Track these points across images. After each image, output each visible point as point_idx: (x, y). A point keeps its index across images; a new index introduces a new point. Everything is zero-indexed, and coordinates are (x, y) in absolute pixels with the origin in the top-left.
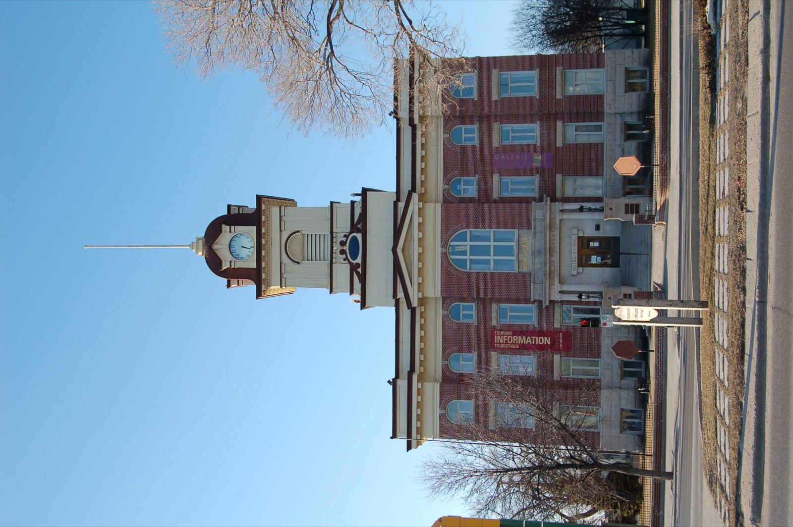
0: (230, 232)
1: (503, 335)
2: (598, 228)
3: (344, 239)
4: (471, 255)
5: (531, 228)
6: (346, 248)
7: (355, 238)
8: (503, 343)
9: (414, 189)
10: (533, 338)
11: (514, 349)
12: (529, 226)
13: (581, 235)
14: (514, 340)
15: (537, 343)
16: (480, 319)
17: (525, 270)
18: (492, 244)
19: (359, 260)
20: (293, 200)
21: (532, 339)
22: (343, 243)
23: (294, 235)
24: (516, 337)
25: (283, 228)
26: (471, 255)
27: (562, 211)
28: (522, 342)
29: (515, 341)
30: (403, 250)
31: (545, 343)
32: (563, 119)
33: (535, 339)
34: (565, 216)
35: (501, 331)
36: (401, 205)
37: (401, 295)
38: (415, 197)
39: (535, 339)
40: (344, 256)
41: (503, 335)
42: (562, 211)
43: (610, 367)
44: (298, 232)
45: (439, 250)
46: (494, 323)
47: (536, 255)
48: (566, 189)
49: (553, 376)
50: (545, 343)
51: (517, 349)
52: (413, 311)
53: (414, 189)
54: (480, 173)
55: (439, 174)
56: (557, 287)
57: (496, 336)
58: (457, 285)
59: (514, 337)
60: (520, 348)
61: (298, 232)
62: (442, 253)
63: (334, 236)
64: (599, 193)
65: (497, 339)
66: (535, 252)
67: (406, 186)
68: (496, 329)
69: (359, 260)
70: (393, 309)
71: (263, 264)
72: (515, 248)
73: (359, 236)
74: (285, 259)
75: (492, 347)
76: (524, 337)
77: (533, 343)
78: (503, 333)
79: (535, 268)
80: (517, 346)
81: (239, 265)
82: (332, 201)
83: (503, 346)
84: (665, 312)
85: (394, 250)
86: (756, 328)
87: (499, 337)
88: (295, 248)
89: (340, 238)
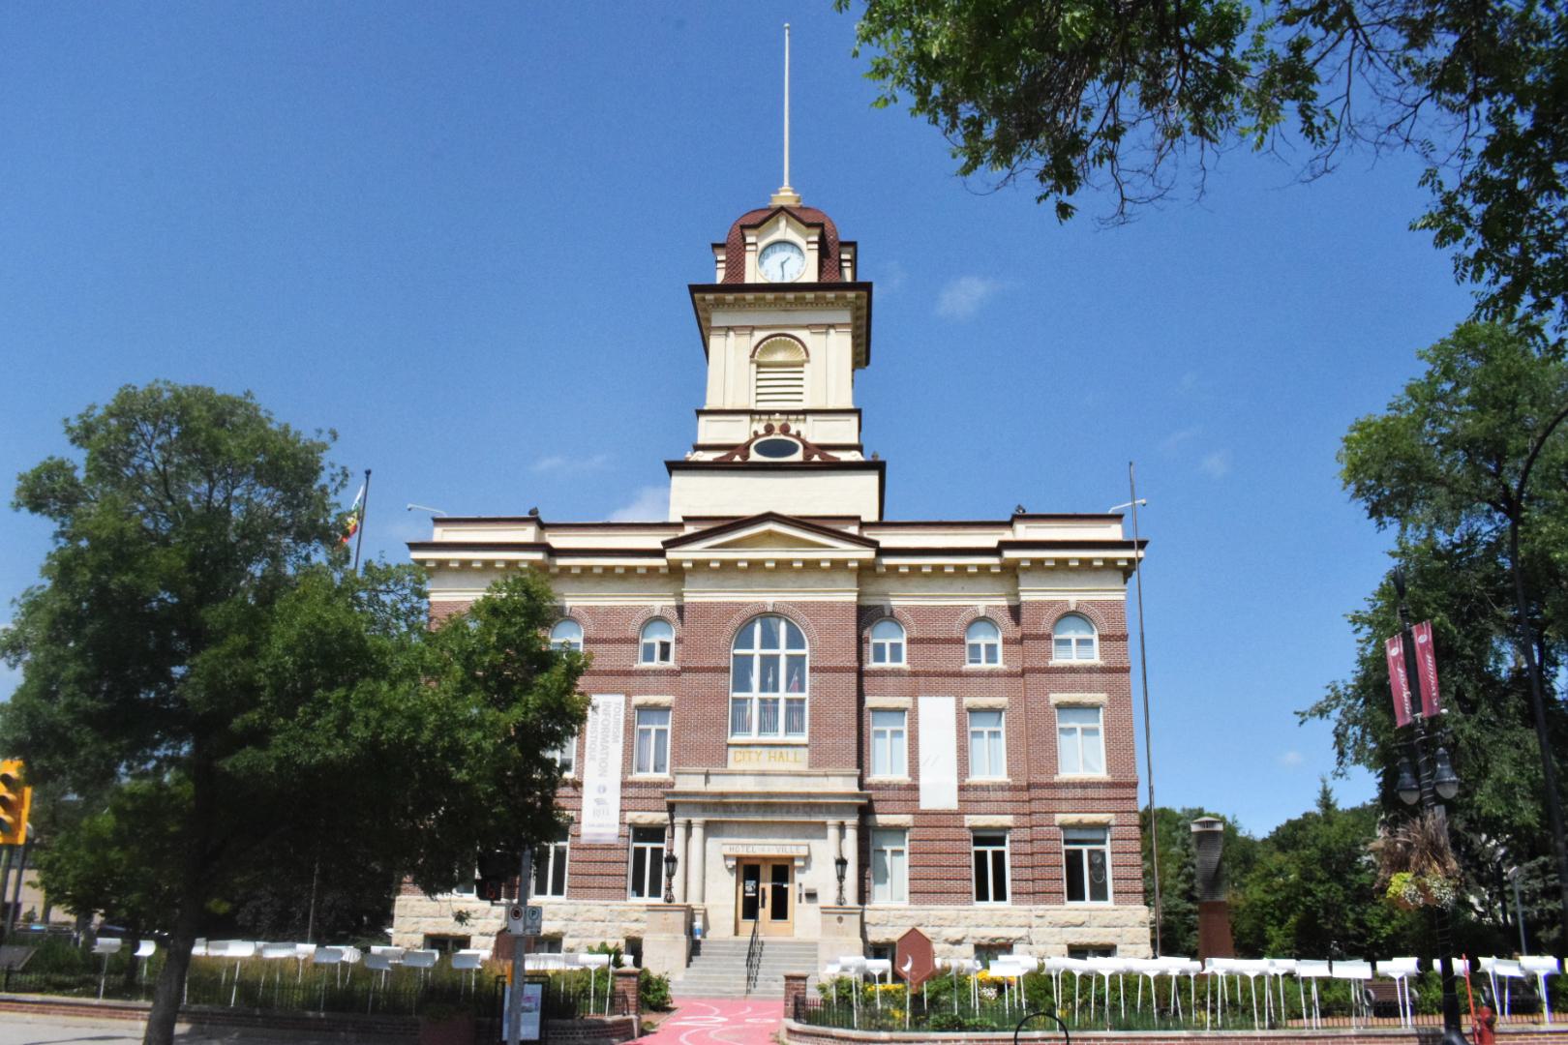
2: (812, 896)
3: (793, 431)
4: (763, 657)
6: (777, 436)
7: (793, 449)
12: (814, 763)
13: (797, 863)
17: (736, 760)
18: (782, 695)
19: (754, 457)
20: (867, 363)
22: (785, 430)
26: (763, 657)
27: (842, 827)
30: (770, 534)
34: (833, 833)
36: (853, 530)
37: (689, 530)
38: (869, 554)
40: (762, 431)
42: (842, 827)
48: (720, 778)
52: (995, 552)
53: (882, 552)
54: (915, 674)
64: (679, 481)
71: (750, 296)
73: (798, 457)
74: (759, 335)
81: (750, 259)
82: (875, 289)
86: (814, 819)
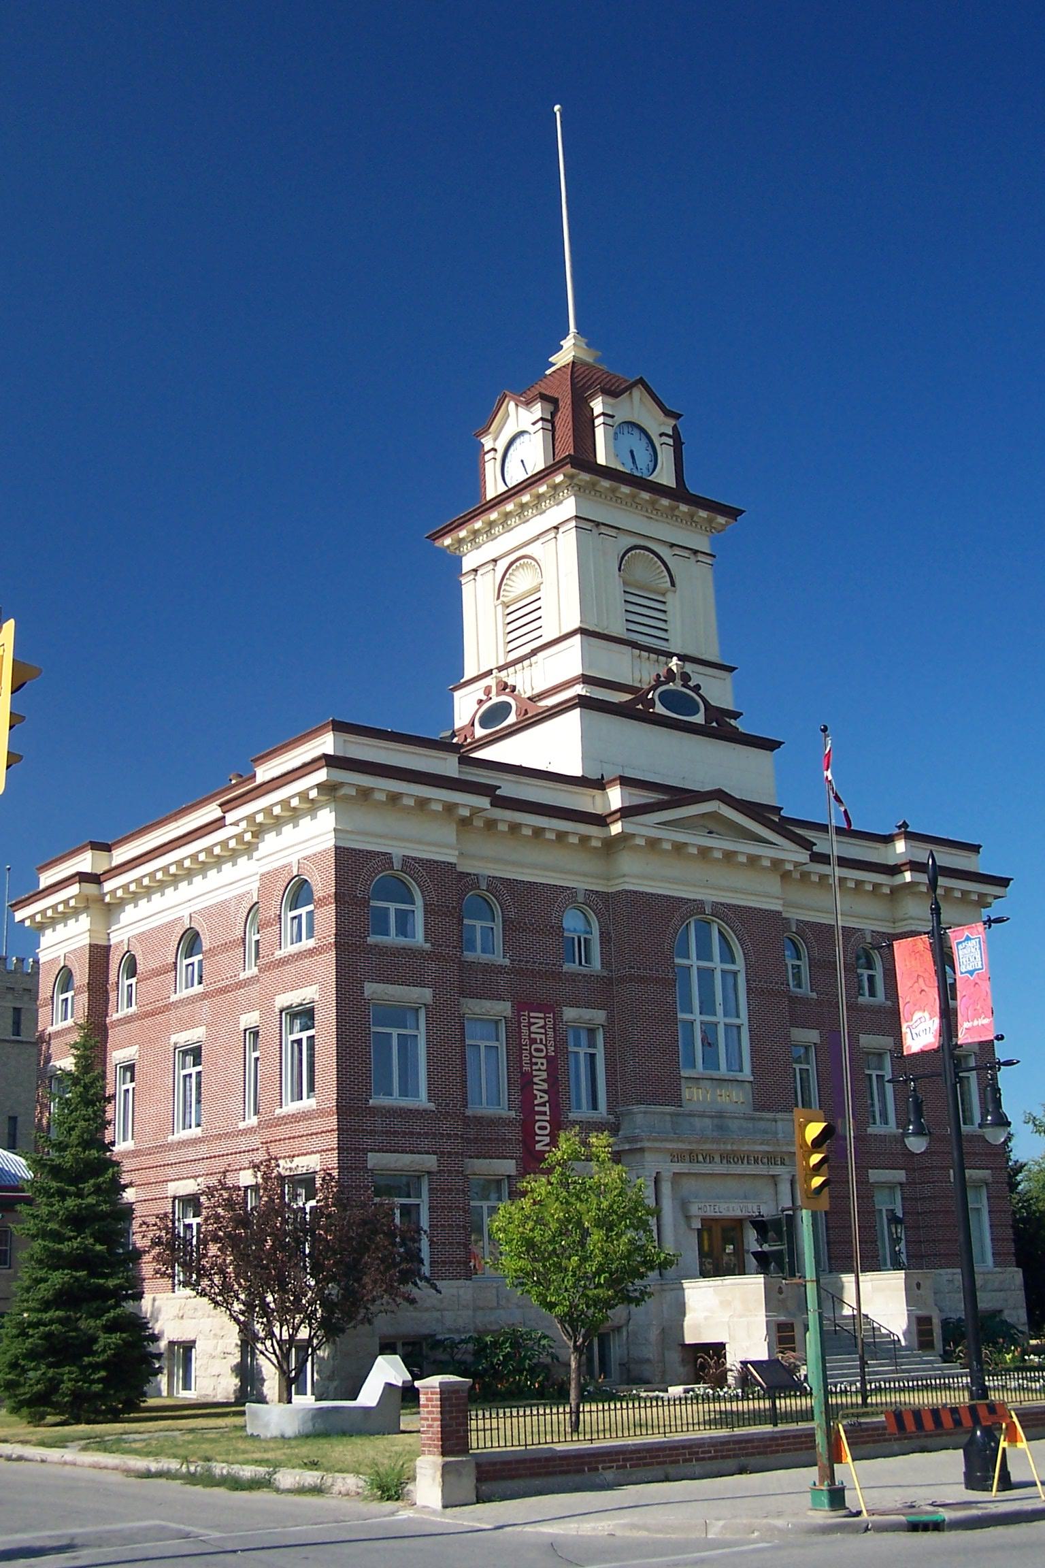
0: (661, 435)
1: (546, 1034)
5: (755, 1110)
8: (530, 1033)
9: (501, 803)
10: (547, 1109)
11: (521, 1060)
12: (760, 1106)
14: (539, 1061)
15: (537, 1117)
16: (574, 981)
19: (660, 709)
21: (543, 1104)
22: (686, 677)
23: (666, 573)
24: (544, 1067)
25: (603, 529)
28: (536, 1080)
29: (536, 1064)
31: (537, 1138)
32: (910, 1183)
33: (544, 1113)
35: (554, 1028)
39: (544, 1113)
41: (546, 1034)
43: (503, 1303)
44: (673, 584)
45: (708, 896)
46: (570, 1013)
47: (716, 1121)
49: (471, 1157)
50: (537, 1138)
51: (522, 1067)
53: (501, 803)
55: (739, 896)
56: (669, 1168)
57: (542, 1015)
58: (646, 928)
59: (544, 1061)
60: (524, 1074)
61: (673, 584)
62: (702, 902)
63: (661, 658)
65: (538, 1020)
66: (721, 1117)
67: (510, 788)
68: (558, 1018)
69: (660, 709)
70: (577, 771)
72: (715, 1074)
75: (523, 1006)
76: (545, 1086)
77: (537, 1108)
78: (551, 1033)
79: (694, 1116)
80: (526, 1068)
83: (525, 1031)
84: (851, 1431)
85: (720, 795)
87: (542, 1022)
88: (645, 569)
89: (698, 675)
